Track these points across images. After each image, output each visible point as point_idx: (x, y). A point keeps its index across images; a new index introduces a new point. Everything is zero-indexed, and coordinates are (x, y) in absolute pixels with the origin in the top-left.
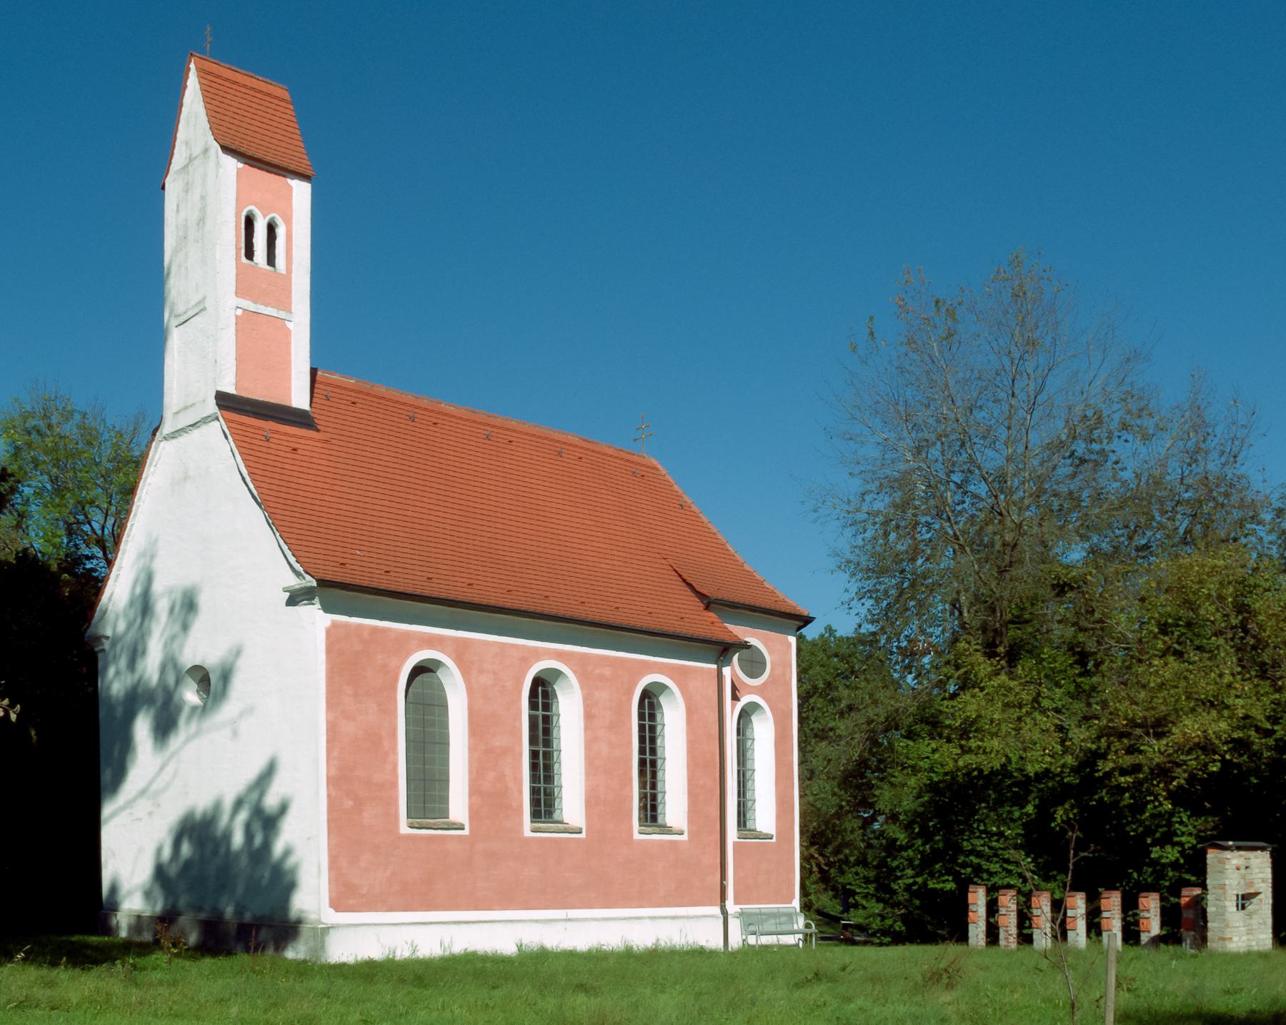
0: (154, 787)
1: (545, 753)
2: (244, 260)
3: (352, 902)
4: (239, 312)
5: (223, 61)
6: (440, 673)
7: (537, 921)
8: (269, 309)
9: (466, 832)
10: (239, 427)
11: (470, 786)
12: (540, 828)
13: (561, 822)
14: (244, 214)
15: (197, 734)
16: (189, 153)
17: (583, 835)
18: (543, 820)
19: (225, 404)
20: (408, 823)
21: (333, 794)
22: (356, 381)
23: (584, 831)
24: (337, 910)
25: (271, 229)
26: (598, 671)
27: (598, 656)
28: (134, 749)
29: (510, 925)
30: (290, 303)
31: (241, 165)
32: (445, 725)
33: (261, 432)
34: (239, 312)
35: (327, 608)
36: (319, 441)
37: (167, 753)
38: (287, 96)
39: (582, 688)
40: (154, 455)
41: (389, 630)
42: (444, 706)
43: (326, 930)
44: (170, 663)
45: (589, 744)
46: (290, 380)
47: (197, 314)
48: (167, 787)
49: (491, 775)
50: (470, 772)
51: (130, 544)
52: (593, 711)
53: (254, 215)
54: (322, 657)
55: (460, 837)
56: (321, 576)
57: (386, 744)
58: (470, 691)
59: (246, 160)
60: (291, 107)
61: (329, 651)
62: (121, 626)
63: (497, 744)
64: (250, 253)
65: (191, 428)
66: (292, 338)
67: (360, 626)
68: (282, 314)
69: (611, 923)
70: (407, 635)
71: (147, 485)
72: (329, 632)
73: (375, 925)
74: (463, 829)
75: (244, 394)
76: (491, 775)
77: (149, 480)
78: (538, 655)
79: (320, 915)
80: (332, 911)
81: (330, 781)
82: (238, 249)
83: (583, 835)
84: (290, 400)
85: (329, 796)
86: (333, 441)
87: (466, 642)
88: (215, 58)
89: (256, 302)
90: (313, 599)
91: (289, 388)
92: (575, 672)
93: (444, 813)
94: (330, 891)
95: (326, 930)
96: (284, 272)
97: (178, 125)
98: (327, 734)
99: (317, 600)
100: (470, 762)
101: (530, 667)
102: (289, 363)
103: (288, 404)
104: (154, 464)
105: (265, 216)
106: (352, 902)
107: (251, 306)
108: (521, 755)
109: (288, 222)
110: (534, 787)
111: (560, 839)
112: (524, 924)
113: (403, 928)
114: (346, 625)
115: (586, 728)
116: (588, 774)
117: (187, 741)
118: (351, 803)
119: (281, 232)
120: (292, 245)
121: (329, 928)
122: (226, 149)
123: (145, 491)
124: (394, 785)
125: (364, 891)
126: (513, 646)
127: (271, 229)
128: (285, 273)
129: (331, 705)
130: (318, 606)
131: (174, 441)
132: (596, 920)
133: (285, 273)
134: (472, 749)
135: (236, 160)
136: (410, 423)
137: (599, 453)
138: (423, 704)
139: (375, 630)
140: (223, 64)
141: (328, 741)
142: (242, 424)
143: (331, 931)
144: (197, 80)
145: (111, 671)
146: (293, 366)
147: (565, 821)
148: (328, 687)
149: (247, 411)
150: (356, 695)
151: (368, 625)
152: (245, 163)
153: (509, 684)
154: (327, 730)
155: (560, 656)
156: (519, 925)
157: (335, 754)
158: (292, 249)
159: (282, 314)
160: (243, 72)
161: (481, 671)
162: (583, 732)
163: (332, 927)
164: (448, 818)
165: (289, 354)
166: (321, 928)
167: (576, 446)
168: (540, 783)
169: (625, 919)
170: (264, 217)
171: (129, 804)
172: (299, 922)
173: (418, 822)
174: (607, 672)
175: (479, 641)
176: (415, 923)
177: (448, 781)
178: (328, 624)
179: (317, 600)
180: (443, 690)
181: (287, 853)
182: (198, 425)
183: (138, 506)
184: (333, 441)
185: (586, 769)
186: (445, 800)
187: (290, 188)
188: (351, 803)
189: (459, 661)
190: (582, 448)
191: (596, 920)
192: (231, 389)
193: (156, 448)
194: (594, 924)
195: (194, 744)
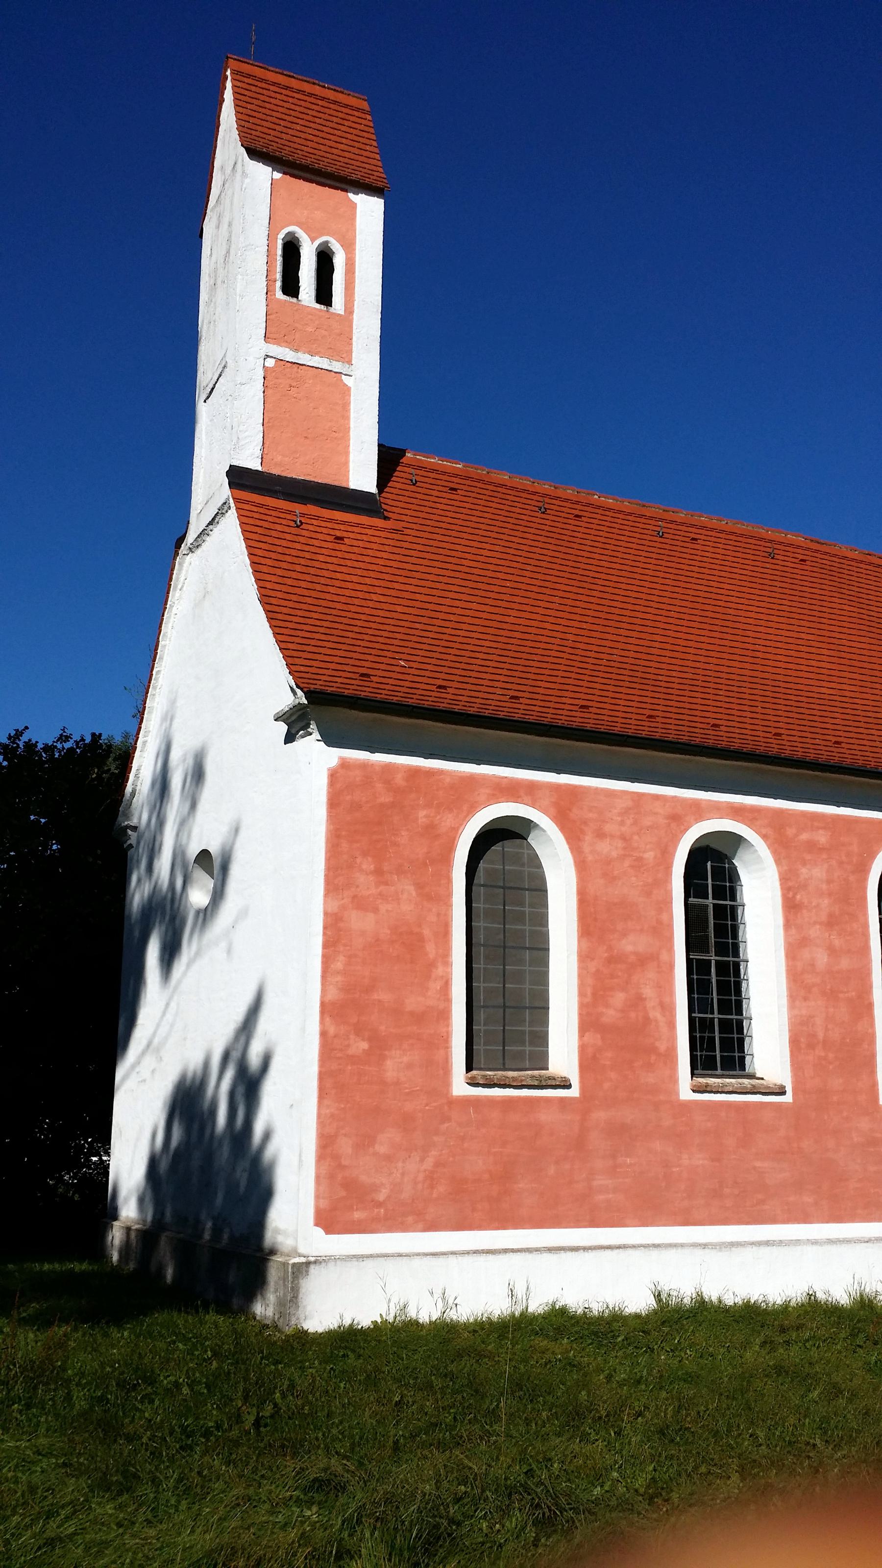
0: (156, 1041)
1: (722, 968)
2: (279, 295)
3: (357, 1215)
4: (270, 363)
5: (271, 66)
6: (533, 840)
7: (704, 1246)
8: (317, 358)
9: (574, 1092)
10: (255, 509)
11: (580, 1015)
12: (707, 1085)
13: (752, 1076)
14: (281, 235)
15: (198, 954)
16: (223, 178)
17: (788, 1098)
18: (719, 1072)
19: (237, 481)
20: (467, 1078)
21: (332, 1030)
22: (463, 466)
23: (789, 1089)
24: (329, 1230)
25: (325, 260)
26: (804, 836)
27: (804, 814)
28: (145, 983)
29: (655, 1253)
30: (350, 352)
31: (277, 175)
32: (541, 919)
33: (288, 517)
34: (270, 363)
35: (331, 739)
36: (384, 529)
37: (171, 989)
38: (365, 105)
39: (778, 862)
40: (178, 574)
41: (441, 772)
42: (540, 890)
43: (302, 1269)
44: (179, 855)
45: (793, 951)
46: (347, 453)
47: (220, 376)
48: (166, 1038)
49: (619, 998)
50: (581, 994)
51: (157, 699)
52: (798, 897)
53: (298, 239)
54: (321, 812)
55: (562, 1100)
56: (318, 686)
57: (431, 949)
58: (581, 866)
59: (286, 170)
60: (369, 117)
61: (333, 803)
62: (145, 817)
63: (629, 948)
64: (291, 286)
65: (211, 527)
66: (352, 398)
67: (388, 768)
68: (337, 366)
69: (844, 1248)
70: (471, 780)
71: (173, 616)
72: (333, 775)
73: (400, 1255)
74: (569, 1087)
75: (276, 471)
76: (619, 998)
77: (174, 610)
78: (699, 811)
79: (296, 1240)
80: (320, 1231)
81: (326, 1009)
82: (270, 281)
83: (788, 1098)
84: (348, 480)
85: (323, 1034)
86: (407, 531)
87: (574, 792)
88: (260, 62)
89: (297, 350)
90: (308, 725)
91: (346, 463)
92: (764, 837)
93: (541, 1060)
94: (317, 1197)
95: (302, 1269)
96: (342, 312)
97: (215, 151)
98: (324, 934)
99: (313, 726)
100: (580, 977)
101: (686, 830)
102: (348, 430)
103: (344, 485)
104: (179, 587)
105: (313, 240)
106: (357, 1215)
107: (288, 355)
108: (671, 966)
109: (349, 246)
110: (544, 986)
111: (747, 1104)
112: (680, 1250)
113: (452, 1259)
114: (364, 765)
115: (788, 925)
116: (792, 998)
117: (189, 965)
118: (364, 1045)
119: (339, 261)
120: (354, 278)
121: (308, 1264)
122: (254, 153)
123: (170, 625)
124: (445, 1015)
125: (381, 1197)
126: (657, 797)
127: (325, 260)
128: (342, 312)
129: (332, 886)
130: (316, 735)
131: (199, 551)
132: (815, 1242)
133: (342, 312)
134: (584, 957)
135: (270, 169)
136: (539, 515)
137: (835, 556)
138: (504, 888)
139: (415, 772)
140: (270, 68)
141: (326, 945)
142: (262, 506)
143: (313, 1269)
144: (231, 91)
145: (134, 878)
146: (352, 434)
147: (758, 1075)
148: (328, 860)
149: (276, 492)
150: (378, 872)
151: (403, 766)
152: (285, 173)
153: (649, 856)
154: (325, 928)
155: (737, 813)
156: (672, 1253)
157: (339, 964)
158: (354, 282)
159: (337, 366)
160: (300, 77)
161: (600, 835)
162: (781, 931)
163: (315, 1262)
164: (547, 1069)
165: (347, 418)
166: (294, 1265)
167: (799, 547)
168: (713, 1013)
169: (550, 1250)
170: (313, 240)
171: (133, 1067)
172: (273, 1252)
173: (484, 1076)
174: (822, 838)
175: (597, 791)
176: (476, 1252)
177: (547, 1008)
178: (334, 762)
179: (313, 726)
180: (539, 866)
181: (267, 1136)
182: (217, 519)
183: (165, 646)
184: (407, 531)
185: (790, 989)
186: (541, 1039)
187: (354, 206)
188: (364, 1045)
189: (562, 819)
190: (808, 549)
191: (815, 1242)
192: (254, 464)
193: (181, 564)
194: (811, 1249)
195: (195, 967)
